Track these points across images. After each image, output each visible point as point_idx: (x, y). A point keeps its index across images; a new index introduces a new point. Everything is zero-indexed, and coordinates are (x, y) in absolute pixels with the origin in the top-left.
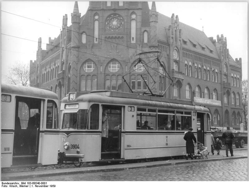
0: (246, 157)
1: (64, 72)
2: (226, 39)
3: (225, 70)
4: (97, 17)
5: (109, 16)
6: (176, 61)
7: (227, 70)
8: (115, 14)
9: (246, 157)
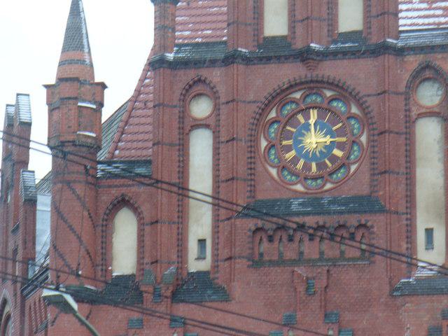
4: (201, 108)
5: (279, 97)
8: (313, 86)
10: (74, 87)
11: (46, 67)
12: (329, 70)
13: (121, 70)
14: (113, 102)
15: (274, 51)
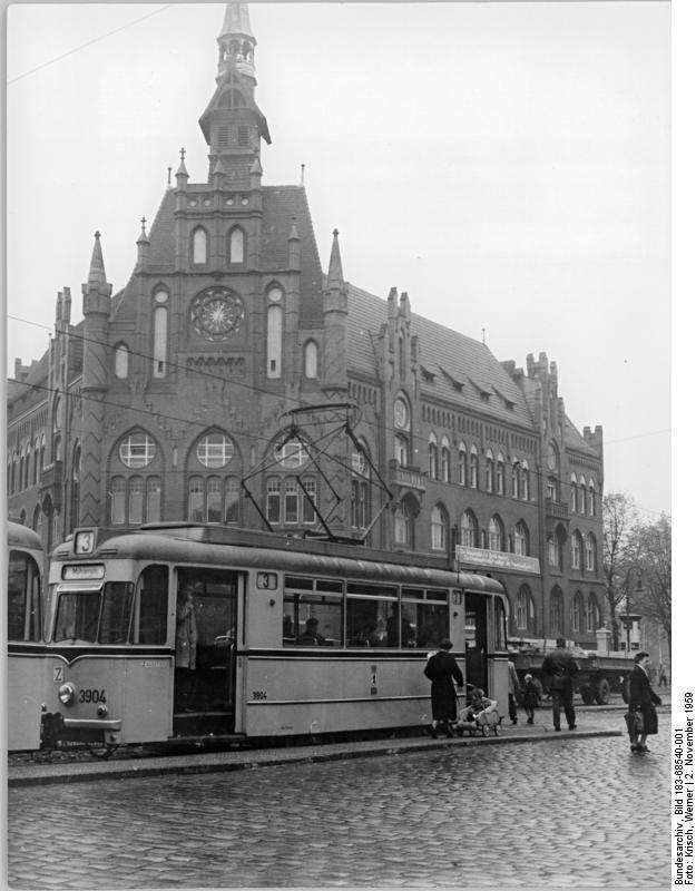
0: (97, 235)
1: (59, 466)
3: (552, 463)
4: (161, 297)
5: (202, 294)
6: (401, 435)
7: (558, 462)
8: (219, 289)
9: (97, 235)
10: (96, 290)
11: (78, 279)
12: (225, 282)
13: (119, 276)
15: (200, 272)
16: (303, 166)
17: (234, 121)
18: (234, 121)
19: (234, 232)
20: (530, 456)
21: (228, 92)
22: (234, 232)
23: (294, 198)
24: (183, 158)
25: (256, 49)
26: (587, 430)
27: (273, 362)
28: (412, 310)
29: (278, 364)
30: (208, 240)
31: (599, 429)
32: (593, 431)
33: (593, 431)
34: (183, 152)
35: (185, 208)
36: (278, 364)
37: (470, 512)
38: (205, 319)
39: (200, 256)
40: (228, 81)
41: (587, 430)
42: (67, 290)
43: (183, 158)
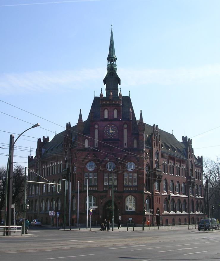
0: (141, 111)
2: (128, 99)
9: (141, 111)
12: (113, 122)
14: (71, 127)
16: (130, 91)
17: (112, 79)
18: (112, 79)
19: (112, 105)
20: (185, 165)
21: (111, 72)
22: (112, 105)
23: (127, 100)
24: (101, 91)
25: (117, 61)
26: (198, 157)
27: (125, 144)
28: (136, 119)
29: (126, 145)
30: (108, 111)
31: (202, 156)
32: (200, 157)
33: (200, 157)
34: (102, 89)
35: (98, 102)
36: (126, 145)
37: (172, 181)
38: (107, 132)
39: (106, 116)
40: (111, 70)
41: (198, 157)
42: (40, 139)
43: (101, 91)
